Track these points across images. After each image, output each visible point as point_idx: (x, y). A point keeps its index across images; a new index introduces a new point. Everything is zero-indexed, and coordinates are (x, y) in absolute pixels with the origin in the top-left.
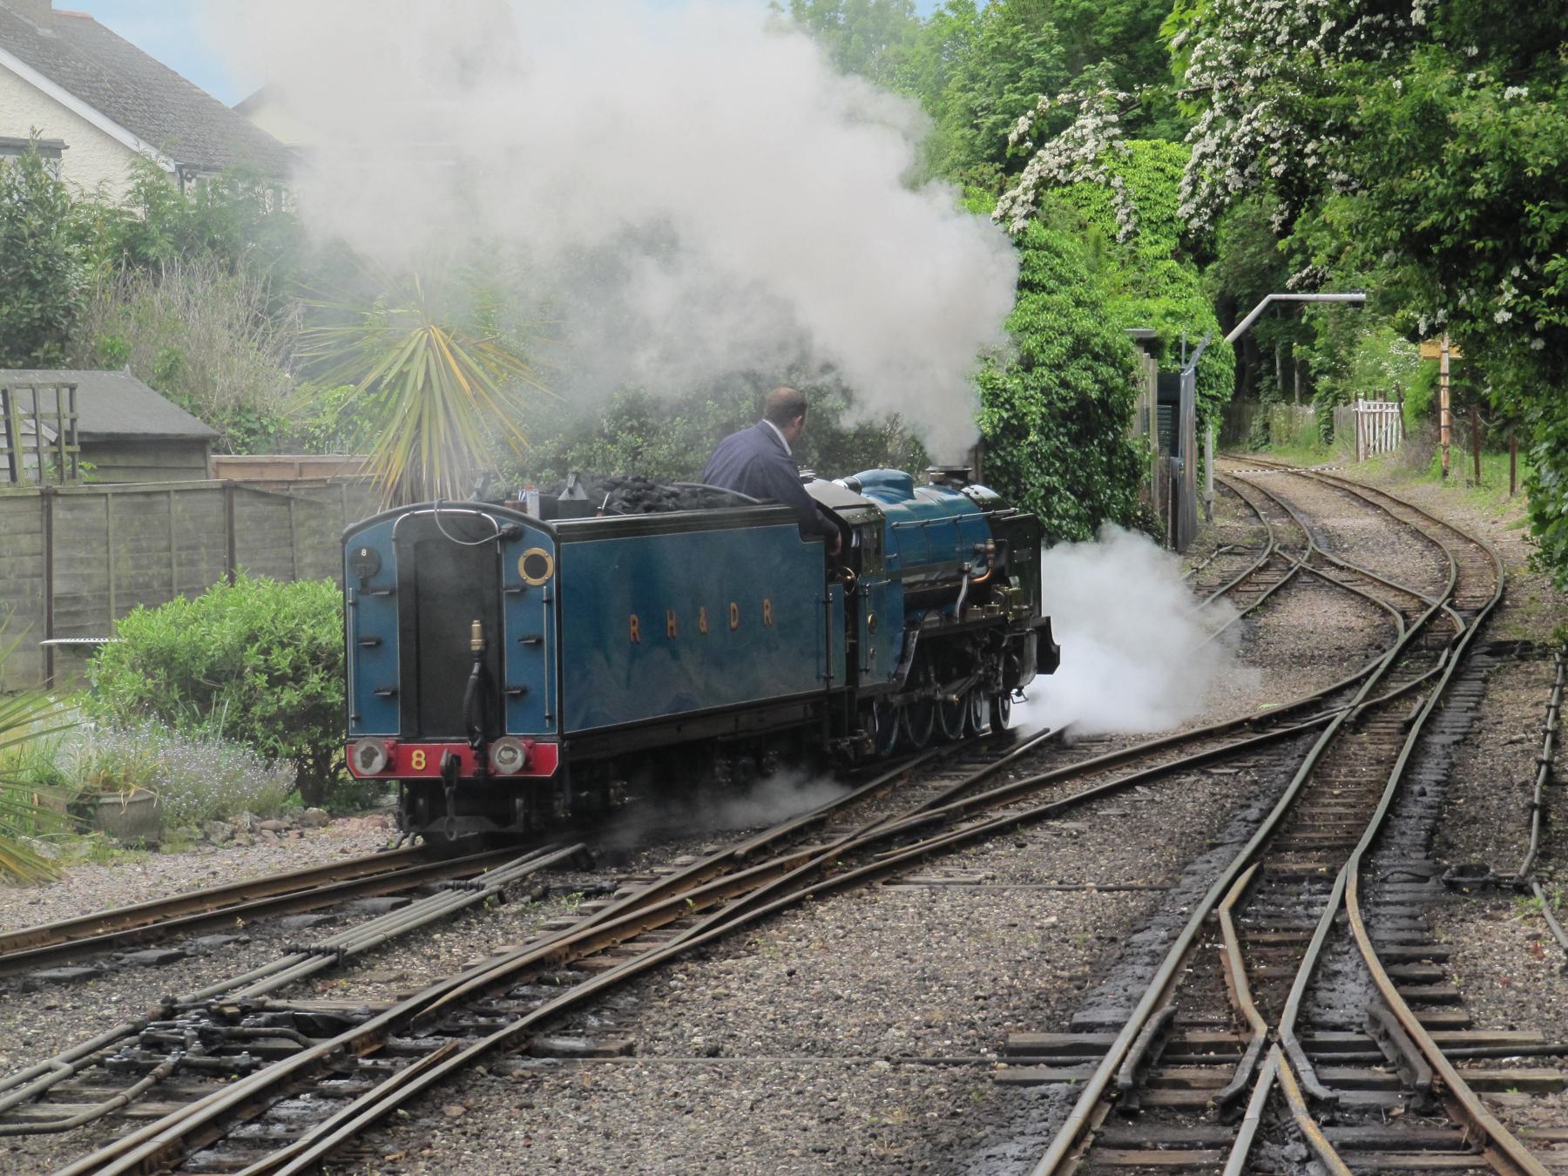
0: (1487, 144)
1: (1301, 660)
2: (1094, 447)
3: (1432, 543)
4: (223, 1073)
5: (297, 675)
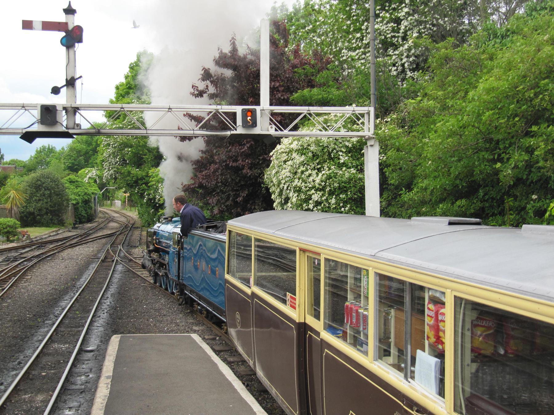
0: (135, 175)
1: (112, 229)
2: (87, 205)
3: (126, 217)
4: (16, 261)
5: (6, 228)
